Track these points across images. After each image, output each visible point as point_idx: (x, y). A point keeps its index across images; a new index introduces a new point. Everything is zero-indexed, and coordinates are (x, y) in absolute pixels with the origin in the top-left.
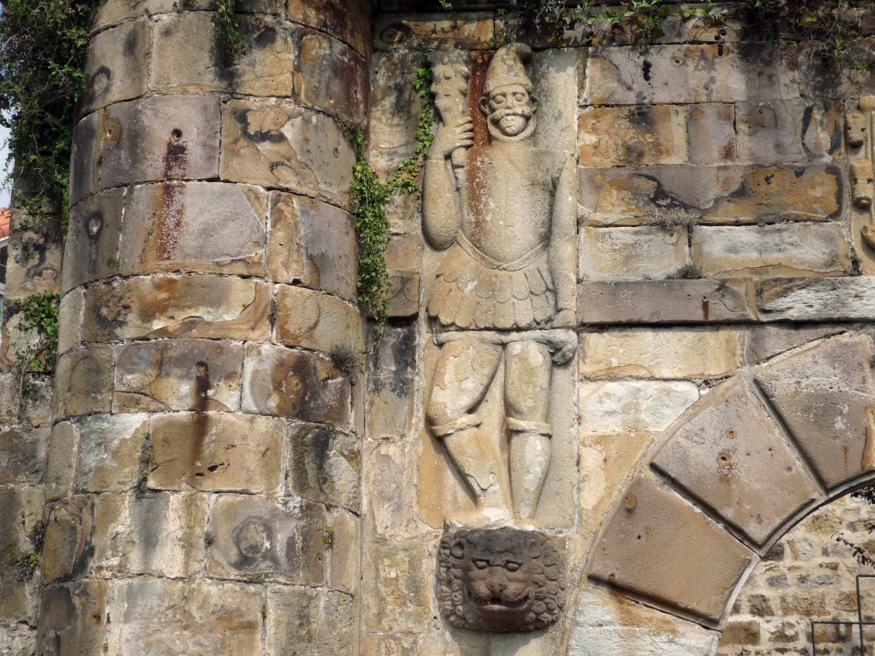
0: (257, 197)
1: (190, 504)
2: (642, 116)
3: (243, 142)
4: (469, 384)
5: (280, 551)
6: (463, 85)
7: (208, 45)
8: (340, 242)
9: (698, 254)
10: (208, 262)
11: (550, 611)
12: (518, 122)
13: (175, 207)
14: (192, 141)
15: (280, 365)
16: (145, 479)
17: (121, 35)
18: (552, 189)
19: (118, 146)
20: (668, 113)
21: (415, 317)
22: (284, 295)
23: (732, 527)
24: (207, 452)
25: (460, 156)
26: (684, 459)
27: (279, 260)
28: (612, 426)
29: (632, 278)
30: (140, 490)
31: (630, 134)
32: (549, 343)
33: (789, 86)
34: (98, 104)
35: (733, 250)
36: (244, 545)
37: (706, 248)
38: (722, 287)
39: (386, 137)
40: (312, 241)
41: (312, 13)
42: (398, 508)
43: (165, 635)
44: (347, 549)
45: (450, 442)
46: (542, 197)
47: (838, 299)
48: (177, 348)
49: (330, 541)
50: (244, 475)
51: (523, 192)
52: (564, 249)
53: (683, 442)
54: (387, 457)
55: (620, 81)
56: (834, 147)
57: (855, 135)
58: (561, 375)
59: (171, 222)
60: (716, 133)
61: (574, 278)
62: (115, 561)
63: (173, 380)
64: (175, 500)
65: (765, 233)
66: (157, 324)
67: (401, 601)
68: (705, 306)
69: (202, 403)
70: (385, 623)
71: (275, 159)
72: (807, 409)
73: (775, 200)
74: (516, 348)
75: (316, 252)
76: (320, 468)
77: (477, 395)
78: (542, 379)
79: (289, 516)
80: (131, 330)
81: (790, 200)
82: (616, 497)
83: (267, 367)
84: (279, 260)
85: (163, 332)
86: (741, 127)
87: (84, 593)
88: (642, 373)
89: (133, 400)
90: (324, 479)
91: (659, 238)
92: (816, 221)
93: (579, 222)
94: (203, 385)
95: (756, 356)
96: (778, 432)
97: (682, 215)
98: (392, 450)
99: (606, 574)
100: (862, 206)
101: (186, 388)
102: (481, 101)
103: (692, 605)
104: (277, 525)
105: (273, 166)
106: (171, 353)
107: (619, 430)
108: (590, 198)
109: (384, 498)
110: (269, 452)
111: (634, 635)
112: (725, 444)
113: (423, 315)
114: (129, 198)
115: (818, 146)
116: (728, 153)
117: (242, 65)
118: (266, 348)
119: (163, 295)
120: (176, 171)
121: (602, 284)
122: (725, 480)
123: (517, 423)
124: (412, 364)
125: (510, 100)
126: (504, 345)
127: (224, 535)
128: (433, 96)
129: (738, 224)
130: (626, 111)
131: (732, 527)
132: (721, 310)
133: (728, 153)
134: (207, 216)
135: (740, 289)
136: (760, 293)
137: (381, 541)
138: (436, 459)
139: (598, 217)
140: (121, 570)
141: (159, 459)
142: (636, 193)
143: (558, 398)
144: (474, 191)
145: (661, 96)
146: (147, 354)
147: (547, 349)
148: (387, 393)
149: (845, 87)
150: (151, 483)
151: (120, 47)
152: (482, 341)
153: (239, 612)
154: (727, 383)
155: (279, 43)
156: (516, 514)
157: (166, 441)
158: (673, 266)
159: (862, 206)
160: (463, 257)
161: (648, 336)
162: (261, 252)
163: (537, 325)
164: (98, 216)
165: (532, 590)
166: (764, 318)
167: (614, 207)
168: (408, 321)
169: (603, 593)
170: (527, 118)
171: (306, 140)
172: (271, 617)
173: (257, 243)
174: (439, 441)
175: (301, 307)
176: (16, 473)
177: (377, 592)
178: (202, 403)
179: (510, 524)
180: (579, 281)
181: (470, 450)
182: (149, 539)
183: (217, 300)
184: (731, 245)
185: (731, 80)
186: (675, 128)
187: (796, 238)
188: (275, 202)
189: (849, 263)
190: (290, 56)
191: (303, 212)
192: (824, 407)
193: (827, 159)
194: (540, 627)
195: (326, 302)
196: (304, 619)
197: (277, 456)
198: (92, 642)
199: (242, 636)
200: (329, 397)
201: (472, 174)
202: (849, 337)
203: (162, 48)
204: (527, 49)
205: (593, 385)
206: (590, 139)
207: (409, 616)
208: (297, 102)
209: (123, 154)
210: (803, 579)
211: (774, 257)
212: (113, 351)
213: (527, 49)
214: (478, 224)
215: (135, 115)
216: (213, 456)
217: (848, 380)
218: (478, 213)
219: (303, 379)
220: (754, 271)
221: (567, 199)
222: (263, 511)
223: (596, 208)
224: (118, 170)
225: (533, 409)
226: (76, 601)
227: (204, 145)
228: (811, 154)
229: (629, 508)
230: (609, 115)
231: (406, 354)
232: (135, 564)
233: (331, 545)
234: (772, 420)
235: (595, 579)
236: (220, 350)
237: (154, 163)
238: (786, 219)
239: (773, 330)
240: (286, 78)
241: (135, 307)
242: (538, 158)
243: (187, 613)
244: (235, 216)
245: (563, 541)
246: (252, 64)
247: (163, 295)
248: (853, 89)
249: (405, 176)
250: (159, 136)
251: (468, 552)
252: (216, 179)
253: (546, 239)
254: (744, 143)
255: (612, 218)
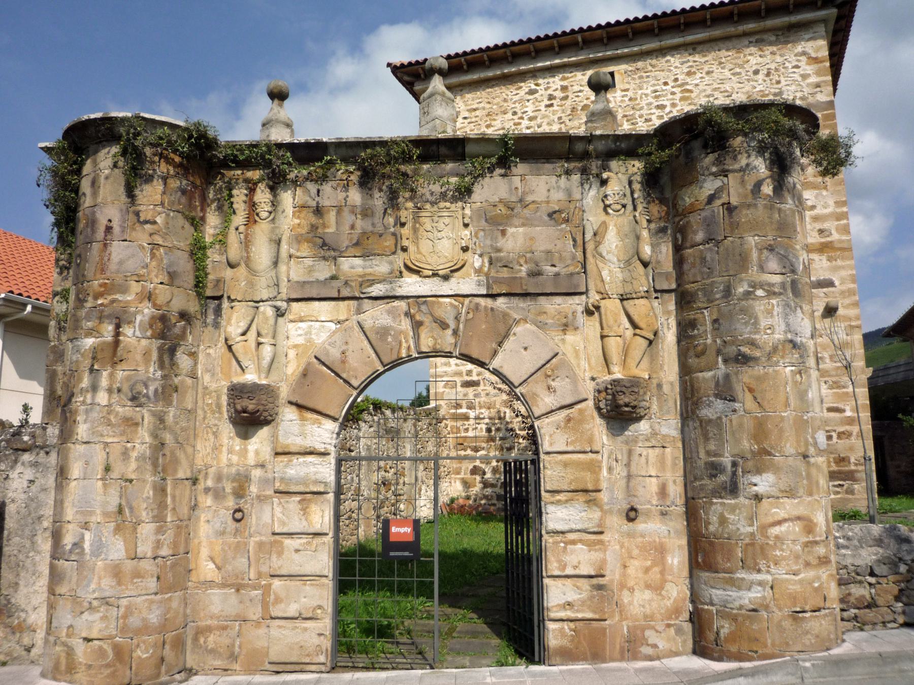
0: (143, 248)
1: (112, 376)
2: (318, 211)
3: (137, 224)
4: (242, 324)
5: (151, 393)
6: (244, 198)
7: (123, 184)
8: (184, 265)
9: (338, 269)
10: (121, 276)
11: (271, 416)
12: (267, 214)
13: (108, 252)
14: (116, 225)
15: (153, 318)
16: (93, 365)
17: (90, 178)
18: (278, 242)
19: (87, 226)
20: (329, 211)
21: (222, 296)
22: (155, 288)
23: (346, 381)
24: (119, 354)
25: (242, 229)
26: (327, 354)
27: (153, 274)
28: (300, 341)
29: (311, 280)
30: (92, 370)
31: (313, 219)
32: (275, 307)
33: (379, 200)
34: (81, 208)
35: (352, 268)
36: (134, 391)
37: (341, 267)
38: (346, 283)
39: (213, 220)
40: (169, 266)
41: (171, 168)
42: (213, 375)
43: (100, 429)
44: (186, 392)
45: (233, 347)
46: (274, 246)
47: (392, 288)
48: (107, 311)
49: (176, 390)
50: (135, 363)
51: (266, 244)
52: (283, 268)
53: (327, 347)
54: (209, 354)
55: (310, 197)
56: (395, 225)
57: (403, 220)
58: (280, 320)
59: (106, 259)
60: (348, 218)
61: (286, 280)
62: (81, 399)
63: (105, 325)
64: (105, 374)
65: (365, 261)
66: (100, 302)
67: (213, 412)
68: (339, 291)
69: (117, 334)
70: (206, 422)
71: (152, 231)
72: (377, 333)
73: (370, 247)
74: (262, 309)
75: (171, 270)
76: (172, 359)
77: (245, 328)
78: (272, 321)
79: (155, 379)
80: (89, 305)
81: (376, 247)
82: (301, 369)
83: (147, 318)
84: (153, 274)
85: (102, 305)
86: (359, 216)
87: (70, 412)
88: (313, 319)
89: (90, 333)
90: (173, 364)
91: (323, 263)
92: (386, 255)
93: (290, 257)
94: (118, 326)
95: (359, 311)
96: (366, 342)
97: (332, 253)
98: (211, 351)
99: (294, 400)
100: (404, 250)
101: (111, 328)
102: (252, 206)
103: (328, 413)
104: (150, 383)
105: (151, 235)
106: (105, 313)
107: (303, 342)
108: (295, 246)
109: (207, 371)
110: (146, 354)
111: (304, 425)
112: (344, 347)
113: (225, 296)
114: (90, 248)
115: (389, 224)
116: (353, 227)
117: (137, 192)
118: (146, 311)
119: (102, 289)
120: (109, 237)
121: (298, 282)
122: (343, 362)
123: (261, 340)
124: (221, 316)
125: (263, 205)
126: (257, 308)
127: (125, 388)
128: (232, 203)
129: (355, 257)
130: (312, 209)
131: (346, 381)
132: (345, 293)
133: (353, 227)
134: (121, 256)
135: (353, 284)
136: (361, 285)
137: (206, 388)
138: (230, 355)
139: (299, 254)
140: (84, 402)
141: (99, 357)
142: (315, 245)
143: (279, 329)
144: (247, 243)
145: (326, 203)
146: (95, 314)
147: (274, 309)
148: (210, 328)
149: (401, 200)
150: (96, 367)
151: (89, 184)
152: (248, 306)
153: (131, 419)
154: (347, 323)
155: (155, 181)
156: (259, 377)
157: (102, 350)
158: (328, 275)
159: (404, 250)
160: (242, 270)
161: (316, 304)
162: (145, 270)
163: (270, 299)
164: (79, 256)
165: (261, 408)
166: (362, 296)
167: (305, 250)
168: (219, 298)
169: (294, 408)
170: (270, 213)
171: (167, 223)
172: (146, 420)
173: (143, 267)
174: (230, 348)
175: (163, 293)
176: (57, 362)
177: (203, 409)
178: (117, 334)
179: (257, 381)
180: (289, 281)
181: (240, 351)
182: (94, 388)
183: (124, 290)
184: (352, 265)
185: (355, 196)
186: (332, 216)
187: (377, 263)
188: (152, 250)
189: (398, 273)
190: (161, 188)
191: (166, 254)
192: (384, 332)
193: (392, 230)
194: (267, 423)
195: (176, 291)
196: (162, 420)
197: (150, 355)
198: (73, 431)
199: (133, 428)
200: (177, 330)
201: (246, 237)
202: (396, 303)
203: (105, 184)
204: (271, 183)
205: (294, 324)
206: (297, 221)
207: (216, 418)
208: (163, 207)
209: (89, 229)
210: (487, 394)
211: (369, 270)
212: (83, 313)
213: (271, 183)
214: (248, 257)
215: (94, 213)
216: (121, 356)
217: (394, 321)
218: (248, 253)
219: (163, 323)
220: (360, 276)
221: (284, 247)
222: (144, 378)
223: (298, 250)
224: (87, 236)
225: (267, 334)
226: (68, 415)
227: (121, 226)
228: (386, 228)
229: (305, 375)
230: (305, 211)
231: (218, 312)
232: (89, 401)
233: (177, 391)
234: (364, 338)
235: (290, 403)
236: (125, 312)
237: (100, 234)
238: (375, 255)
239: (366, 301)
240: (158, 197)
241: (91, 294)
242: (273, 230)
243: (109, 420)
244: (133, 256)
245: (279, 388)
246: (142, 191)
247: (102, 289)
248: (404, 200)
249: (220, 237)
250: (103, 222)
251: (237, 391)
252: (126, 240)
253: (276, 264)
254: (360, 223)
255: (304, 255)
